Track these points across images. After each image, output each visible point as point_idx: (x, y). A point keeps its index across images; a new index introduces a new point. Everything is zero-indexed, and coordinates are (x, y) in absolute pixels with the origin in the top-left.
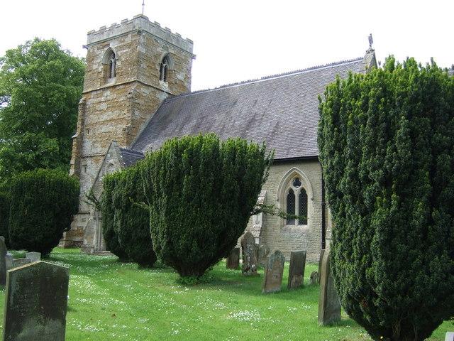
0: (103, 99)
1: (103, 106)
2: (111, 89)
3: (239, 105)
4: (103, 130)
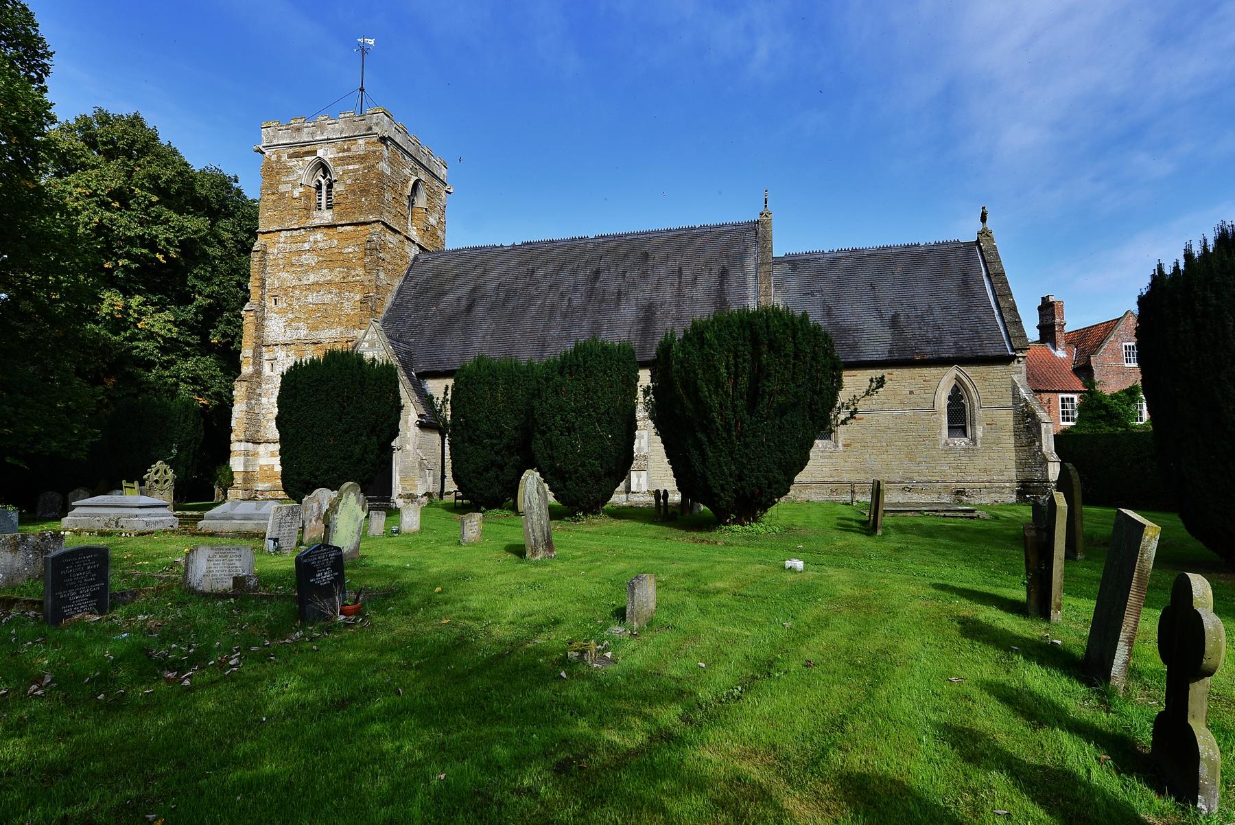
0: (307, 246)
1: (307, 259)
2: (325, 231)
4: (310, 299)
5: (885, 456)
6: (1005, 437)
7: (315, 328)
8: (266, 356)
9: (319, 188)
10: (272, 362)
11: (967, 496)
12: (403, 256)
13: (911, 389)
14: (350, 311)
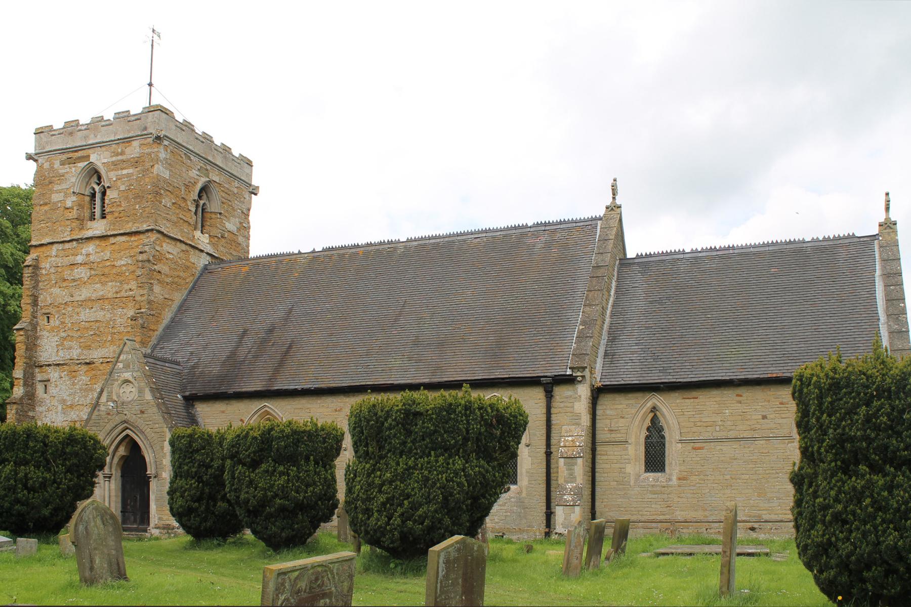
2: (97, 242)
4: (83, 317)
7: (88, 347)
8: (39, 377)
9: (93, 195)
10: (46, 383)
12: (187, 268)
13: (764, 414)
14: (122, 328)
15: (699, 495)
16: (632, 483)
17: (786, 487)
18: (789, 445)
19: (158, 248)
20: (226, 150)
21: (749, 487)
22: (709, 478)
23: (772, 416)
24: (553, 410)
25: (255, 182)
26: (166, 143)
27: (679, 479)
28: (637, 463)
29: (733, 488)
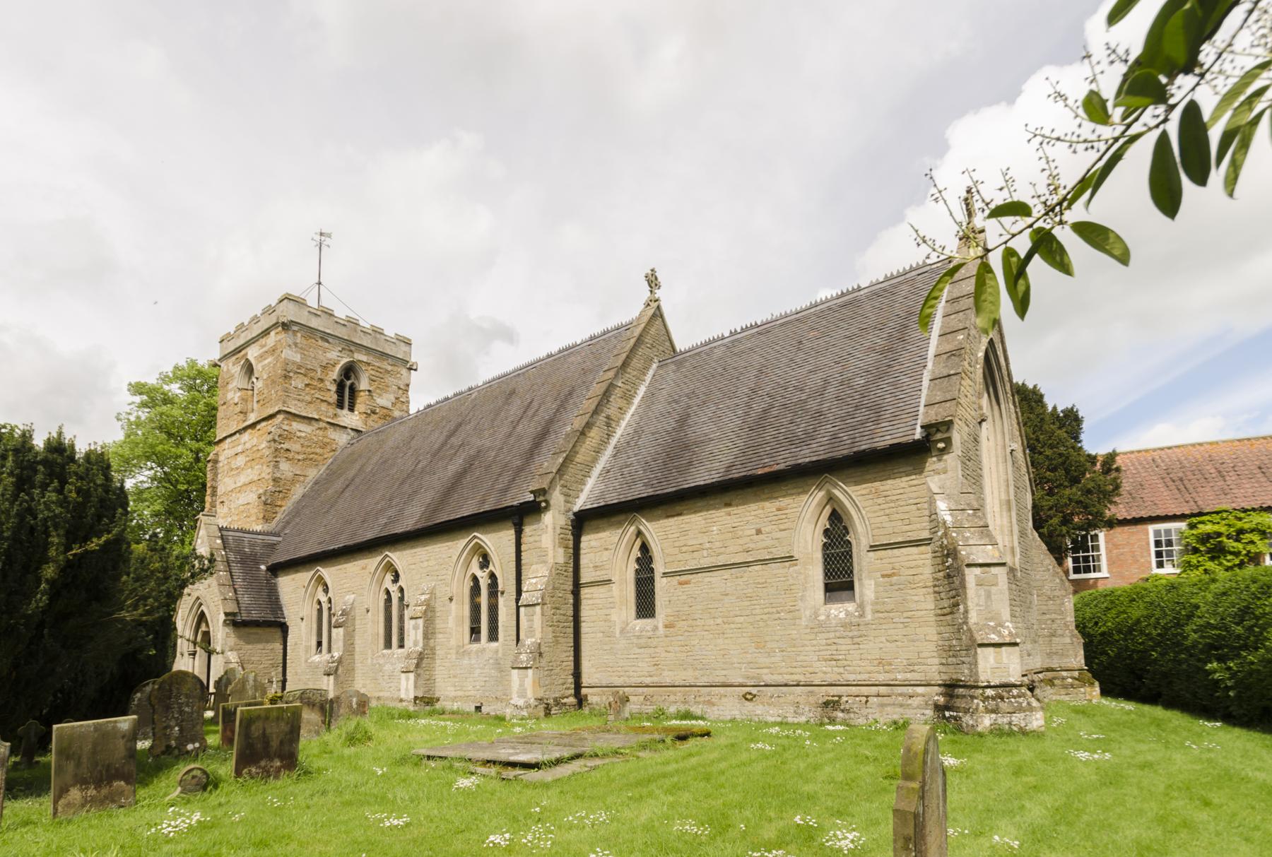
2: (249, 431)
3: (896, 717)
4: (241, 502)
5: (720, 641)
6: (916, 598)
11: (843, 711)
13: (758, 526)
15: (688, 648)
16: (618, 635)
17: (790, 632)
18: (791, 569)
19: (285, 427)
20: (377, 332)
21: (744, 635)
22: (698, 623)
23: (767, 529)
24: (523, 547)
25: (413, 360)
26: (295, 328)
27: (666, 626)
28: (624, 607)
29: (726, 636)
